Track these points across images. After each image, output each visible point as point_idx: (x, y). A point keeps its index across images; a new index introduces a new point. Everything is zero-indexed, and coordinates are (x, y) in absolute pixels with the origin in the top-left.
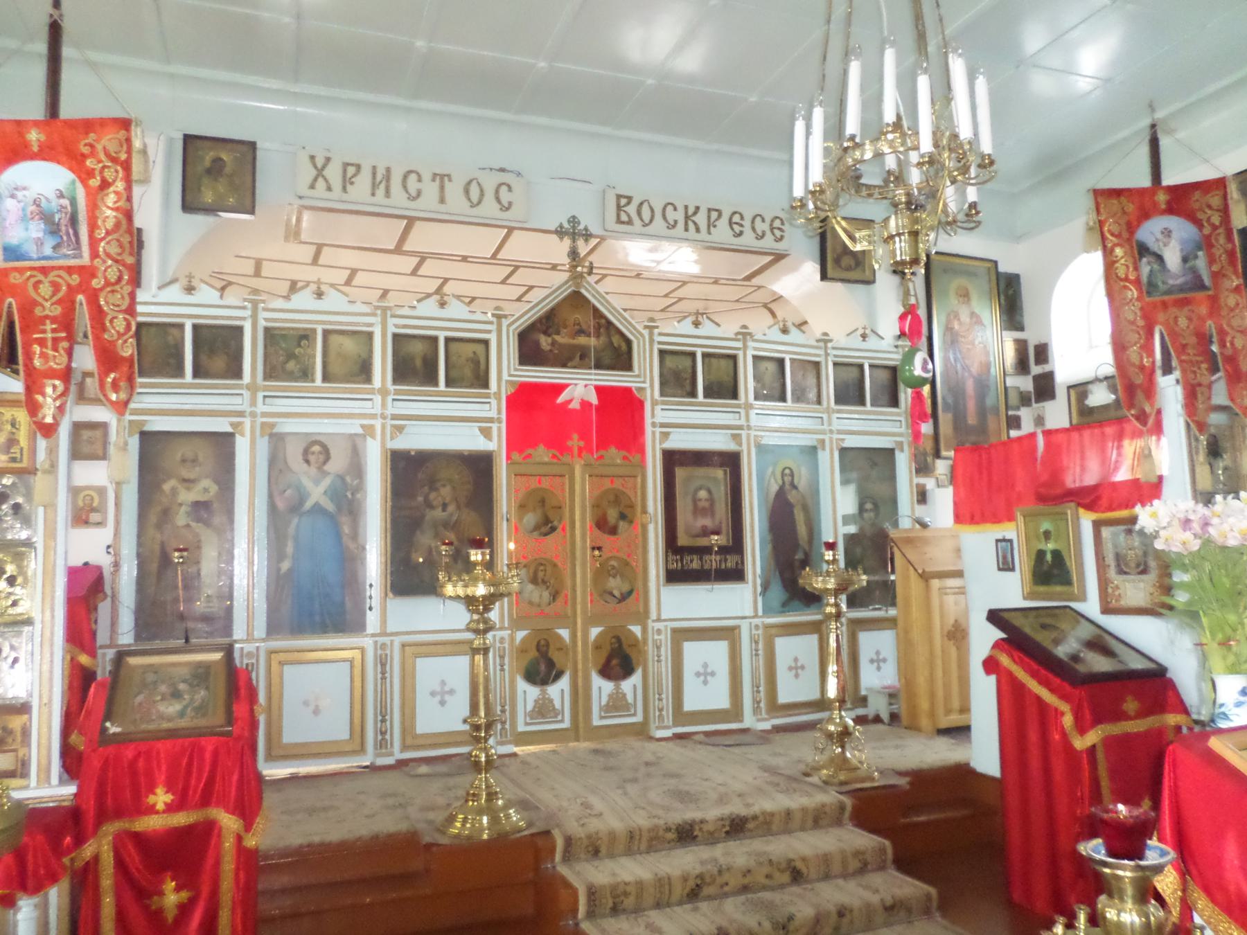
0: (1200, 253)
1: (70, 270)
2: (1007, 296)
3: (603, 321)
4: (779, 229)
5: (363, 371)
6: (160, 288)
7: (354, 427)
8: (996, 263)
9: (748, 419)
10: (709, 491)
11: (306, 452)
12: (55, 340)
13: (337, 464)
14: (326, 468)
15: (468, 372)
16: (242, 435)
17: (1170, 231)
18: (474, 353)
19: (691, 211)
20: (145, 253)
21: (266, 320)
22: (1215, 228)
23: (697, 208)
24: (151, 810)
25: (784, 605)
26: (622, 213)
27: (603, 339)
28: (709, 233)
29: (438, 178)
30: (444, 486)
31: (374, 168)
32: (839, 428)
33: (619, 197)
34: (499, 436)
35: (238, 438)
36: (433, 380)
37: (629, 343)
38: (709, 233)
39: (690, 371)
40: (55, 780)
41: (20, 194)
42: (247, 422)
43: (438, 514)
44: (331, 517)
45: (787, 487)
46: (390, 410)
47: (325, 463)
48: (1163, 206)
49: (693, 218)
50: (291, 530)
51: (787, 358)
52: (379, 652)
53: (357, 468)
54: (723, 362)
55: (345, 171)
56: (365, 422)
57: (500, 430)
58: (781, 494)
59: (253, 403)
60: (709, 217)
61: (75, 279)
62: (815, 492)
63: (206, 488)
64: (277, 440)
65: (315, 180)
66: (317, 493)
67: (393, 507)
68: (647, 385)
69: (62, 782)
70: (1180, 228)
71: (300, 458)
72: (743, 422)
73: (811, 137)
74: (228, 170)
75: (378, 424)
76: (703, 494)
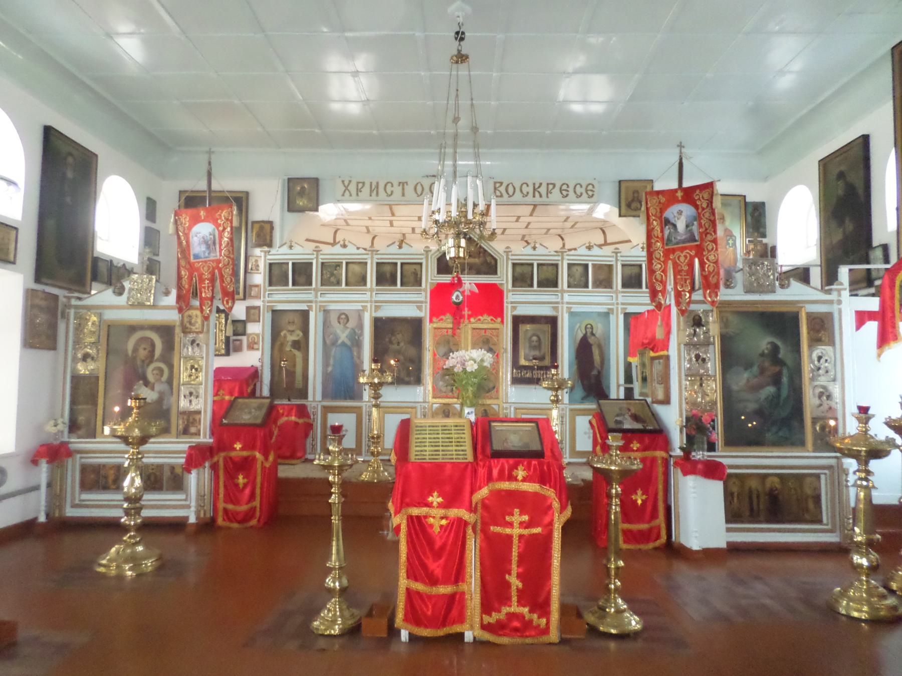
0: (695, 223)
1: (213, 261)
2: (752, 216)
3: (482, 250)
4: (591, 191)
5: (363, 280)
6: (279, 248)
7: (358, 306)
8: (745, 196)
9: (562, 298)
10: (539, 337)
11: (339, 318)
12: (208, 287)
13: (352, 324)
14: (347, 325)
15: (412, 279)
16: (312, 311)
17: (682, 212)
18: (415, 269)
19: (537, 186)
20: (274, 231)
21: (322, 259)
22: (703, 209)
23: (541, 184)
24: (235, 449)
25: (583, 399)
26: (497, 191)
27: (481, 259)
28: (548, 197)
29: (401, 184)
30: (398, 334)
31: (371, 183)
32: (623, 302)
33: (495, 183)
34: (426, 309)
35: (311, 312)
36: (395, 284)
37: (496, 260)
38: (548, 197)
39: (530, 273)
40: (208, 436)
41: (198, 235)
42: (314, 305)
43: (395, 347)
44: (350, 349)
45: (589, 334)
46: (374, 299)
47: (346, 323)
48: (680, 198)
49: (539, 190)
50: (333, 353)
51: (590, 264)
52: (368, 410)
53: (361, 326)
54: (550, 268)
55: (358, 186)
56: (363, 304)
57: (427, 307)
58: (584, 340)
59: (316, 297)
60: (548, 188)
61: (215, 265)
62: (607, 338)
63: (297, 335)
64: (326, 312)
65: (345, 191)
66: (343, 336)
67: (375, 344)
68: (504, 282)
69: (210, 438)
70: (687, 210)
71: (337, 322)
72: (559, 300)
73: (330, 246)
74: (307, 191)
75: (369, 305)
76: (535, 338)
